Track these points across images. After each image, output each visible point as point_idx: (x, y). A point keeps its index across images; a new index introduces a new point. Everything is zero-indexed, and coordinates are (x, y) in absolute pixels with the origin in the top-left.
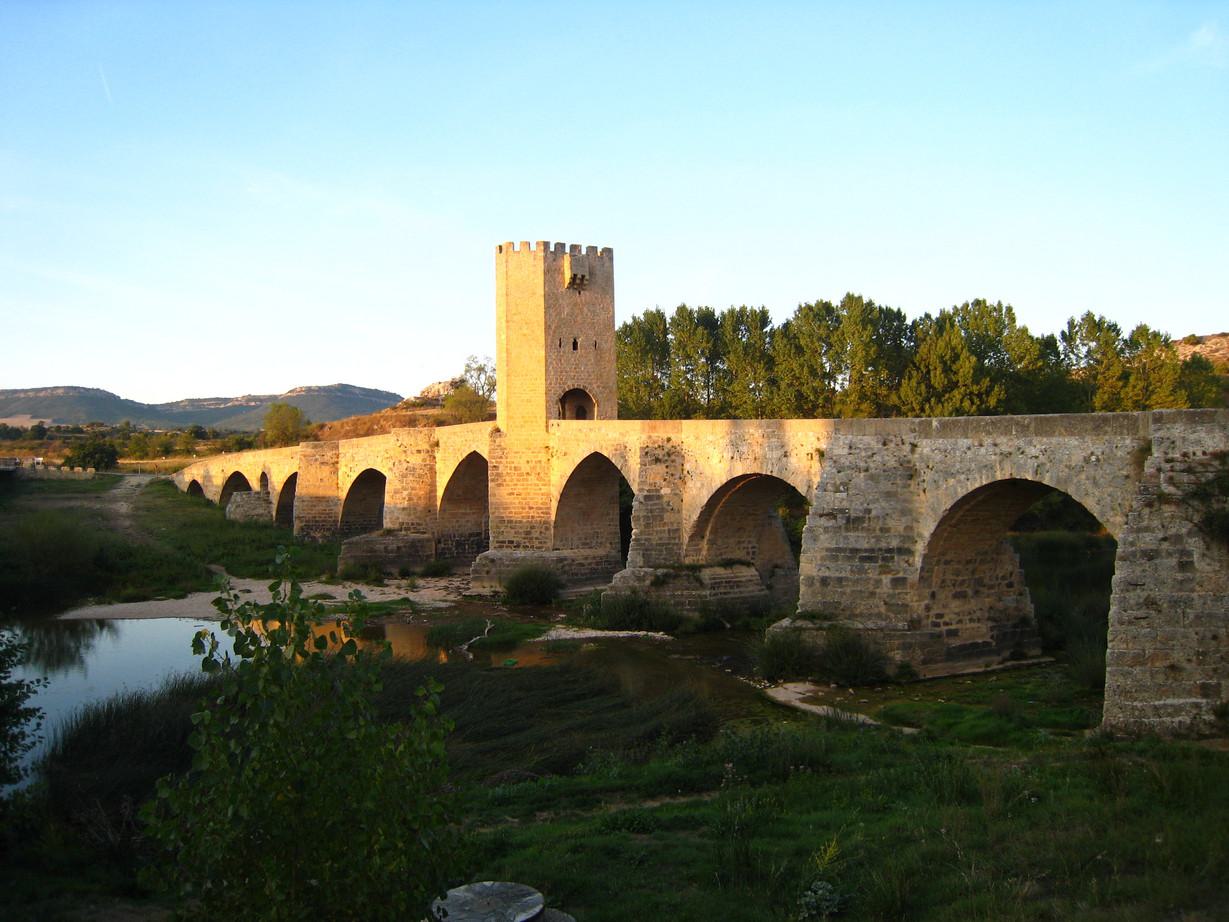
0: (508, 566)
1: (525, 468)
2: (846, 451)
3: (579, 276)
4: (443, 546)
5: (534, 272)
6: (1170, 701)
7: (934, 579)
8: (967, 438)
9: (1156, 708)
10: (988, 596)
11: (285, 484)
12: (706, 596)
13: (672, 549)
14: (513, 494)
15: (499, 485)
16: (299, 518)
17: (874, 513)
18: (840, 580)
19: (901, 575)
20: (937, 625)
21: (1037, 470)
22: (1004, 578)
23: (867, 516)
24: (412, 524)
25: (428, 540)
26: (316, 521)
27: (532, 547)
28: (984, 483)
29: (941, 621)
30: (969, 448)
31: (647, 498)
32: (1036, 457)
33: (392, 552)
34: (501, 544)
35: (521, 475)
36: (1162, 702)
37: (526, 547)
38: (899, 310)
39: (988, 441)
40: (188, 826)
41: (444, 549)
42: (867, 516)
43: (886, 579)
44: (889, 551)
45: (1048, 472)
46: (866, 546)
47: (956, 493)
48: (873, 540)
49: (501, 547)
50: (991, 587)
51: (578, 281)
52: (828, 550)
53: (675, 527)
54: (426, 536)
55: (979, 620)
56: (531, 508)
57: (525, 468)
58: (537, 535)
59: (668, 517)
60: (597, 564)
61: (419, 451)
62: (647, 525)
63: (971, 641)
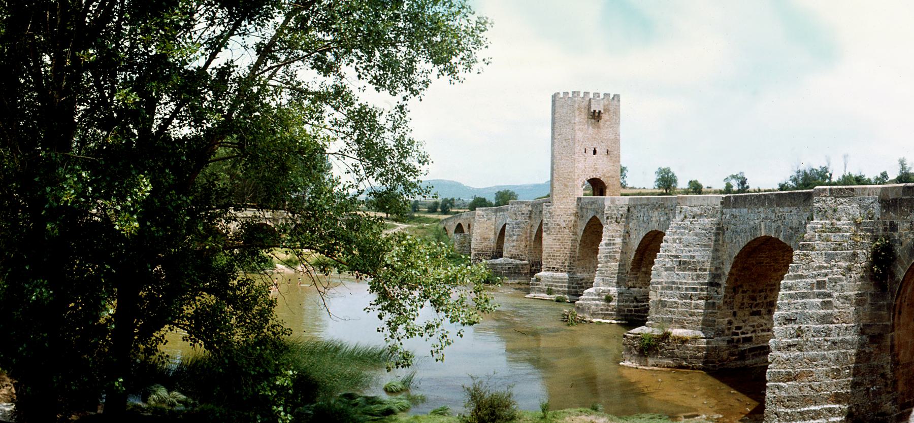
6: (813, 408)
7: (736, 304)
9: (801, 413)
20: (737, 334)
29: (739, 331)
31: (607, 245)
34: (549, 269)
36: (806, 409)
57: (563, 225)
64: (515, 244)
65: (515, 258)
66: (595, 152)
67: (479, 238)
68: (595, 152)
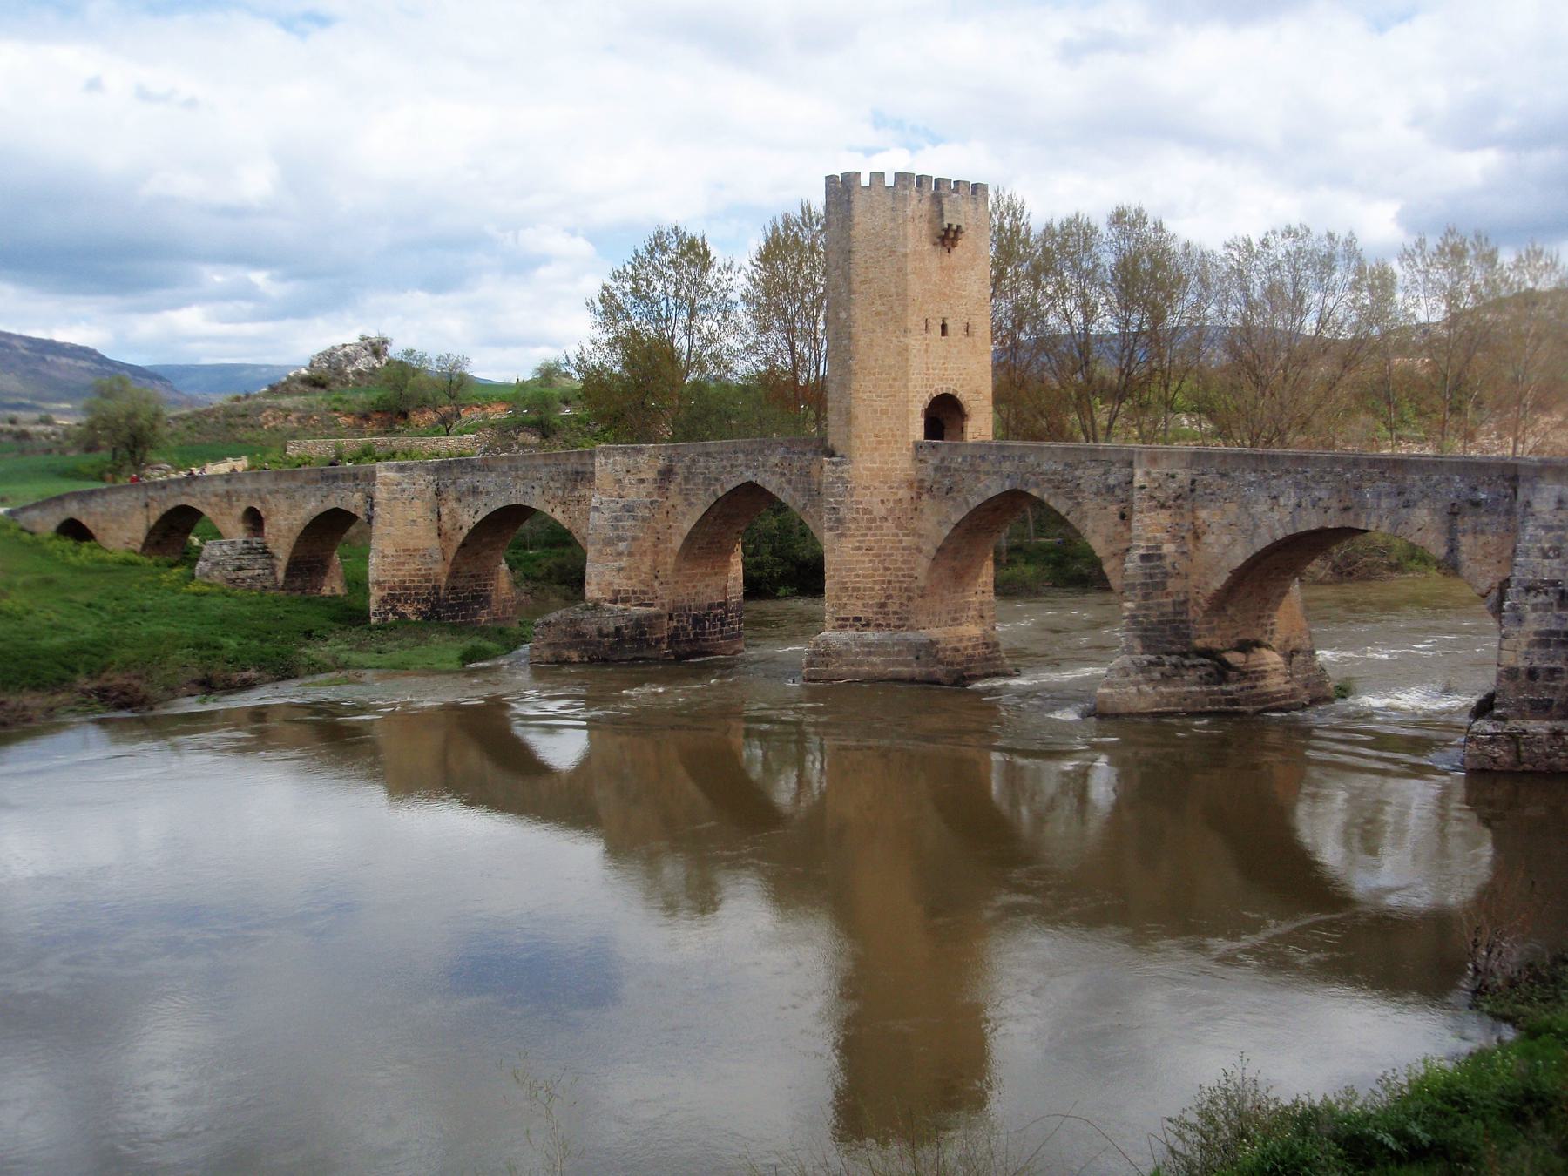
0: (857, 654)
1: (879, 510)
2: (1552, 505)
5: (893, 219)
11: (307, 527)
12: (1230, 693)
13: (1177, 628)
14: (859, 548)
15: (842, 535)
16: (378, 583)
18: (1552, 671)
24: (634, 592)
25: (659, 616)
26: (406, 588)
27: (888, 625)
31: (1144, 558)
33: (607, 636)
34: (843, 623)
35: (873, 520)
37: (879, 626)
38: (1351, 233)
40: (1523, 916)
41: (676, 628)
47: (967, 503)
49: (843, 627)
51: (951, 235)
52: (1536, 633)
53: (1182, 598)
54: (652, 609)
56: (887, 569)
57: (879, 510)
58: (896, 608)
59: (1172, 584)
60: (975, 647)
61: (642, 481)
62: (1146, 596)
64: (624, 562)
65: (625, 600)
67: (390, 551)
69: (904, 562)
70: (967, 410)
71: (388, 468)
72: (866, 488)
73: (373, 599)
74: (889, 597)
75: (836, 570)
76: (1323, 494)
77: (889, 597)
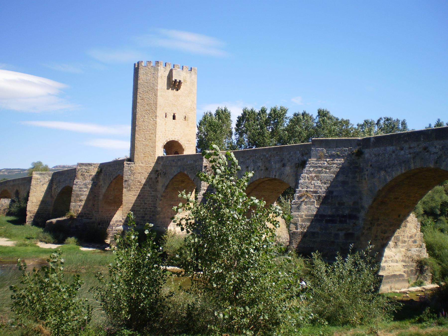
3: (178, 81)
4: (101, 226)
5: (153, 77)
8: (392, 145)
10: (402, 247)
15: (129, 190)
16: (29, 211)
17: (335, 194)
19: (350, 231)
21: (437, 161)
22: (411, 237)
23: (331, 195)
24: (85, 214)
28: (403, 171)
30: (394, 152)
32: (437, 153)
39: (406, 146)
42: (331, 195)
43: (341, 234)
44: (344, 216)
45: (444, 161)
46: (329, 213)
47: (385, 179)
48: (334, 210)
50: (405, 242)
55: (397, 262)
56: (145, 204)
63: (393, 274)
66: (174, 118)
68: (174, 118)
69: (152, 201)
70: (184, 147)
71: (37, 174)
72: (139, 173)
73: (27, 217)
74: (146, 214)
75: (126, 203)
76: (260, 164)
77: (146, 214)
